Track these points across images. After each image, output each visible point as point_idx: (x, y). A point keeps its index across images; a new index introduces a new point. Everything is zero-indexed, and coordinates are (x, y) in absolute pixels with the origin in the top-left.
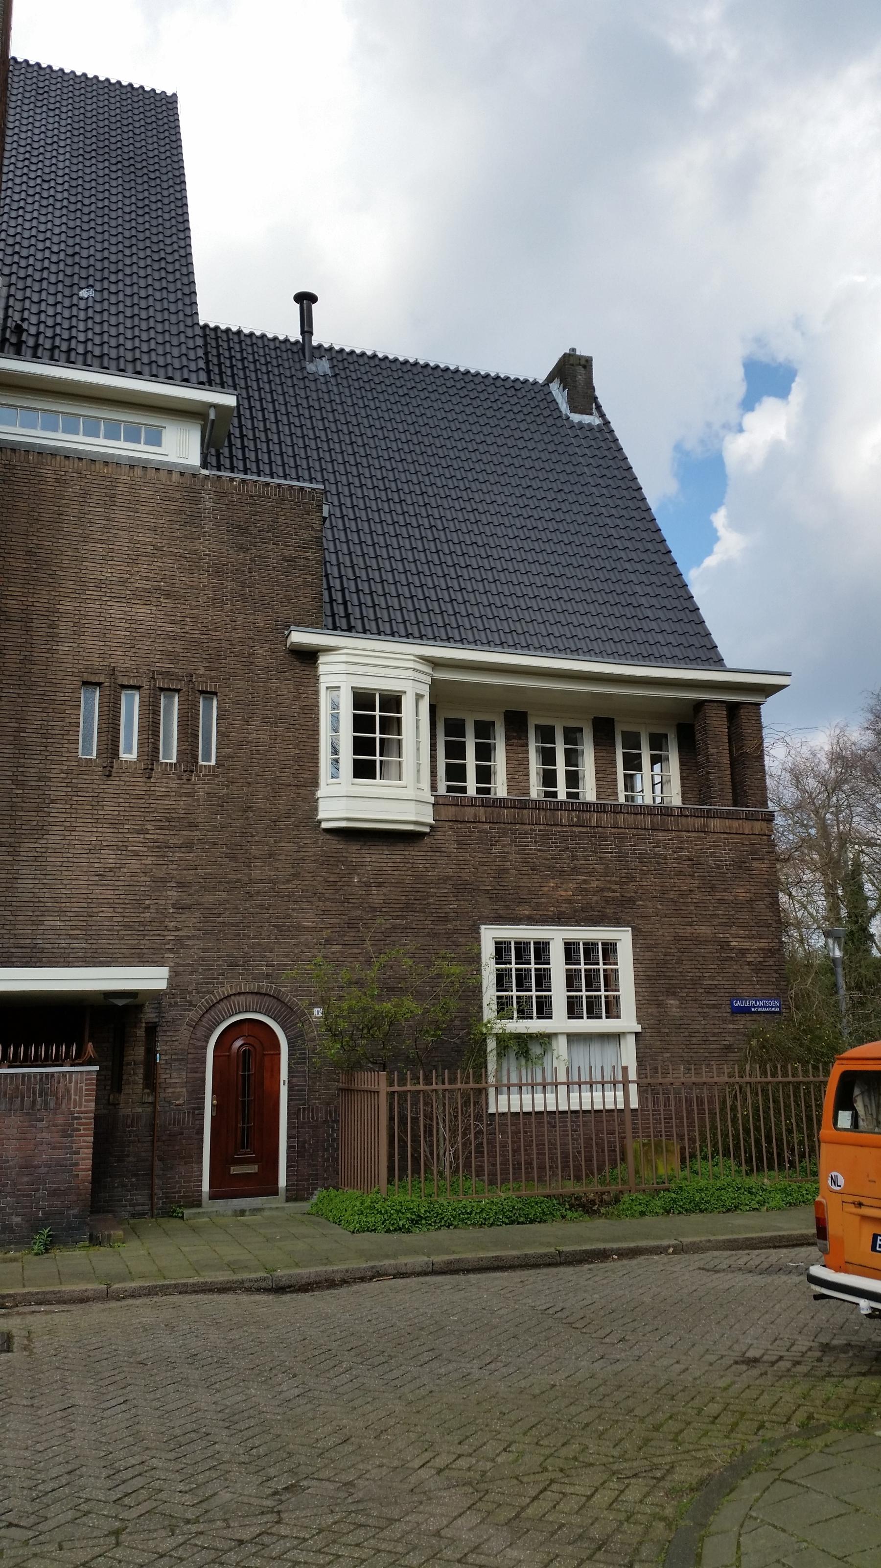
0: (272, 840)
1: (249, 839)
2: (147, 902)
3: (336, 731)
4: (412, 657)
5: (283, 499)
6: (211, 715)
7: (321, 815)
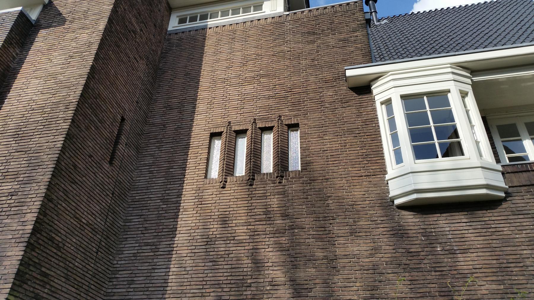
0: (351, 220)
1: (331, 221)
2: (249, 281)
3: (393, 129)
4: (449, 65)
5: (336, 12)
6: (295, 140)
7: (392, 194)
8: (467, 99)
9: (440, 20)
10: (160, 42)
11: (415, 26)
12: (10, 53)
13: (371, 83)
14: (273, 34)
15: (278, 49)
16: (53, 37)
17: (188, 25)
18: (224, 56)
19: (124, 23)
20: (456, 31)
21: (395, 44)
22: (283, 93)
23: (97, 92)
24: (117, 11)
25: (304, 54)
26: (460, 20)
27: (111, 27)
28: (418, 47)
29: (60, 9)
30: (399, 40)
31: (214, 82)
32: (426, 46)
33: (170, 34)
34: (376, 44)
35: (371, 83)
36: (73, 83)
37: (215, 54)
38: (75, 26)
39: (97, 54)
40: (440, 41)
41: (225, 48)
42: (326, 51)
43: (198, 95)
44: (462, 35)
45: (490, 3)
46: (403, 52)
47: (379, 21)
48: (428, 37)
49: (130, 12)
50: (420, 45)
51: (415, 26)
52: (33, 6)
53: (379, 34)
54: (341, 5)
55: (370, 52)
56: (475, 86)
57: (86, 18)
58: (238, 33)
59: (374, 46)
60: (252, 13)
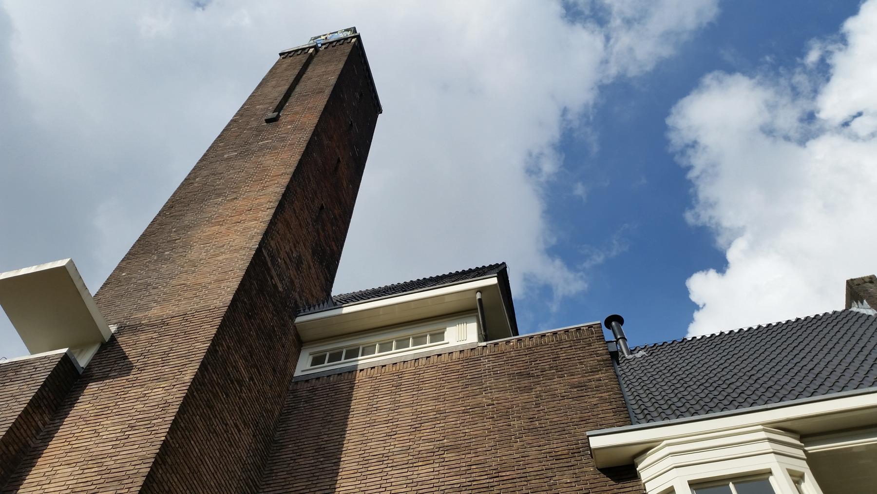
8: (803, 486)
9: (731, 349)
10: (280, 396)
11: (692, 360)
12: (34, 424)
13: (636, 461)
14: (462, 377)
15: (471, 401)
16: (109, 394)
17: (327, 367)
18: (382, 415)
19: (226, 369)
20: (760, 366)
21: (664, 390)
22: (484, 480)
23: (167, 489)
24: (216, 351)
25: (514, 409)
26: (764, 348)
27: (203, 376)
28: (703, 395)
29: (126, 350)
30: (670, 384)
31: (365, 461)
32: (716, 393)
33: (297, 383)
34: (633, 390)
35: (636, 461)
36: (128, 473)
37: (369, 412)
38: (145, 375)
39: (175, 422)
40: (738, 384)
41: (385, 402)
42: (552, 404)
43: (337, 486)
44: (772, 373)
45: (815, 318)
46: (679, 404)
47: (631, 352)
48: (716, 379)
49: (236, 351)
50: (706, 392)
51: (692, 360)
52: (83, 346)
53: (635, 374)
54: (567, 331)
55: (625, 405)
56: (813, 460)
57: (164, 362)
58: (407, 376)
59: (629, 393)
60: (428, 345)
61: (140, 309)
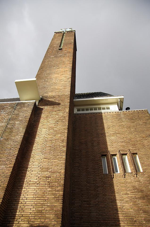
22: (127, 141)
61: (46, 93)
